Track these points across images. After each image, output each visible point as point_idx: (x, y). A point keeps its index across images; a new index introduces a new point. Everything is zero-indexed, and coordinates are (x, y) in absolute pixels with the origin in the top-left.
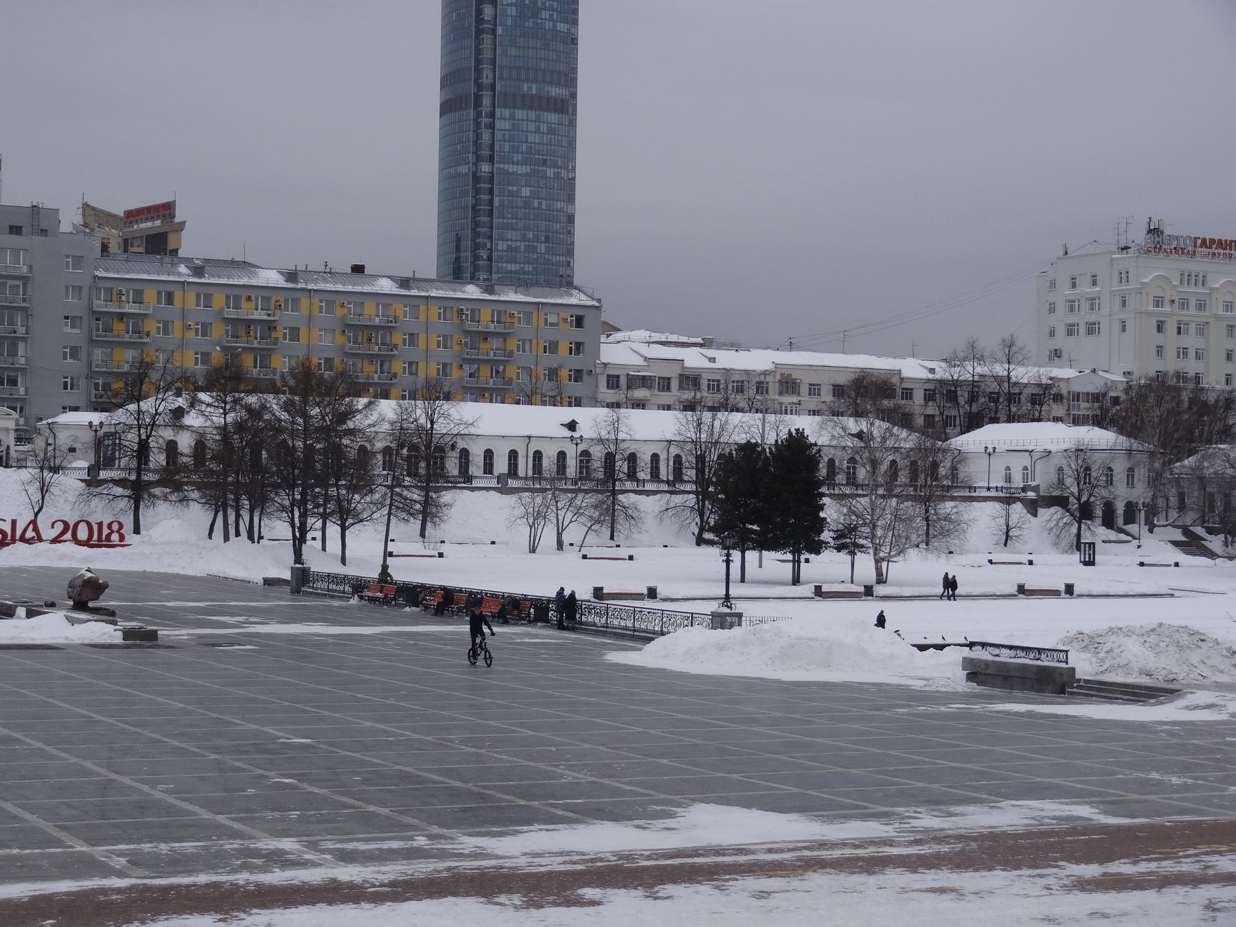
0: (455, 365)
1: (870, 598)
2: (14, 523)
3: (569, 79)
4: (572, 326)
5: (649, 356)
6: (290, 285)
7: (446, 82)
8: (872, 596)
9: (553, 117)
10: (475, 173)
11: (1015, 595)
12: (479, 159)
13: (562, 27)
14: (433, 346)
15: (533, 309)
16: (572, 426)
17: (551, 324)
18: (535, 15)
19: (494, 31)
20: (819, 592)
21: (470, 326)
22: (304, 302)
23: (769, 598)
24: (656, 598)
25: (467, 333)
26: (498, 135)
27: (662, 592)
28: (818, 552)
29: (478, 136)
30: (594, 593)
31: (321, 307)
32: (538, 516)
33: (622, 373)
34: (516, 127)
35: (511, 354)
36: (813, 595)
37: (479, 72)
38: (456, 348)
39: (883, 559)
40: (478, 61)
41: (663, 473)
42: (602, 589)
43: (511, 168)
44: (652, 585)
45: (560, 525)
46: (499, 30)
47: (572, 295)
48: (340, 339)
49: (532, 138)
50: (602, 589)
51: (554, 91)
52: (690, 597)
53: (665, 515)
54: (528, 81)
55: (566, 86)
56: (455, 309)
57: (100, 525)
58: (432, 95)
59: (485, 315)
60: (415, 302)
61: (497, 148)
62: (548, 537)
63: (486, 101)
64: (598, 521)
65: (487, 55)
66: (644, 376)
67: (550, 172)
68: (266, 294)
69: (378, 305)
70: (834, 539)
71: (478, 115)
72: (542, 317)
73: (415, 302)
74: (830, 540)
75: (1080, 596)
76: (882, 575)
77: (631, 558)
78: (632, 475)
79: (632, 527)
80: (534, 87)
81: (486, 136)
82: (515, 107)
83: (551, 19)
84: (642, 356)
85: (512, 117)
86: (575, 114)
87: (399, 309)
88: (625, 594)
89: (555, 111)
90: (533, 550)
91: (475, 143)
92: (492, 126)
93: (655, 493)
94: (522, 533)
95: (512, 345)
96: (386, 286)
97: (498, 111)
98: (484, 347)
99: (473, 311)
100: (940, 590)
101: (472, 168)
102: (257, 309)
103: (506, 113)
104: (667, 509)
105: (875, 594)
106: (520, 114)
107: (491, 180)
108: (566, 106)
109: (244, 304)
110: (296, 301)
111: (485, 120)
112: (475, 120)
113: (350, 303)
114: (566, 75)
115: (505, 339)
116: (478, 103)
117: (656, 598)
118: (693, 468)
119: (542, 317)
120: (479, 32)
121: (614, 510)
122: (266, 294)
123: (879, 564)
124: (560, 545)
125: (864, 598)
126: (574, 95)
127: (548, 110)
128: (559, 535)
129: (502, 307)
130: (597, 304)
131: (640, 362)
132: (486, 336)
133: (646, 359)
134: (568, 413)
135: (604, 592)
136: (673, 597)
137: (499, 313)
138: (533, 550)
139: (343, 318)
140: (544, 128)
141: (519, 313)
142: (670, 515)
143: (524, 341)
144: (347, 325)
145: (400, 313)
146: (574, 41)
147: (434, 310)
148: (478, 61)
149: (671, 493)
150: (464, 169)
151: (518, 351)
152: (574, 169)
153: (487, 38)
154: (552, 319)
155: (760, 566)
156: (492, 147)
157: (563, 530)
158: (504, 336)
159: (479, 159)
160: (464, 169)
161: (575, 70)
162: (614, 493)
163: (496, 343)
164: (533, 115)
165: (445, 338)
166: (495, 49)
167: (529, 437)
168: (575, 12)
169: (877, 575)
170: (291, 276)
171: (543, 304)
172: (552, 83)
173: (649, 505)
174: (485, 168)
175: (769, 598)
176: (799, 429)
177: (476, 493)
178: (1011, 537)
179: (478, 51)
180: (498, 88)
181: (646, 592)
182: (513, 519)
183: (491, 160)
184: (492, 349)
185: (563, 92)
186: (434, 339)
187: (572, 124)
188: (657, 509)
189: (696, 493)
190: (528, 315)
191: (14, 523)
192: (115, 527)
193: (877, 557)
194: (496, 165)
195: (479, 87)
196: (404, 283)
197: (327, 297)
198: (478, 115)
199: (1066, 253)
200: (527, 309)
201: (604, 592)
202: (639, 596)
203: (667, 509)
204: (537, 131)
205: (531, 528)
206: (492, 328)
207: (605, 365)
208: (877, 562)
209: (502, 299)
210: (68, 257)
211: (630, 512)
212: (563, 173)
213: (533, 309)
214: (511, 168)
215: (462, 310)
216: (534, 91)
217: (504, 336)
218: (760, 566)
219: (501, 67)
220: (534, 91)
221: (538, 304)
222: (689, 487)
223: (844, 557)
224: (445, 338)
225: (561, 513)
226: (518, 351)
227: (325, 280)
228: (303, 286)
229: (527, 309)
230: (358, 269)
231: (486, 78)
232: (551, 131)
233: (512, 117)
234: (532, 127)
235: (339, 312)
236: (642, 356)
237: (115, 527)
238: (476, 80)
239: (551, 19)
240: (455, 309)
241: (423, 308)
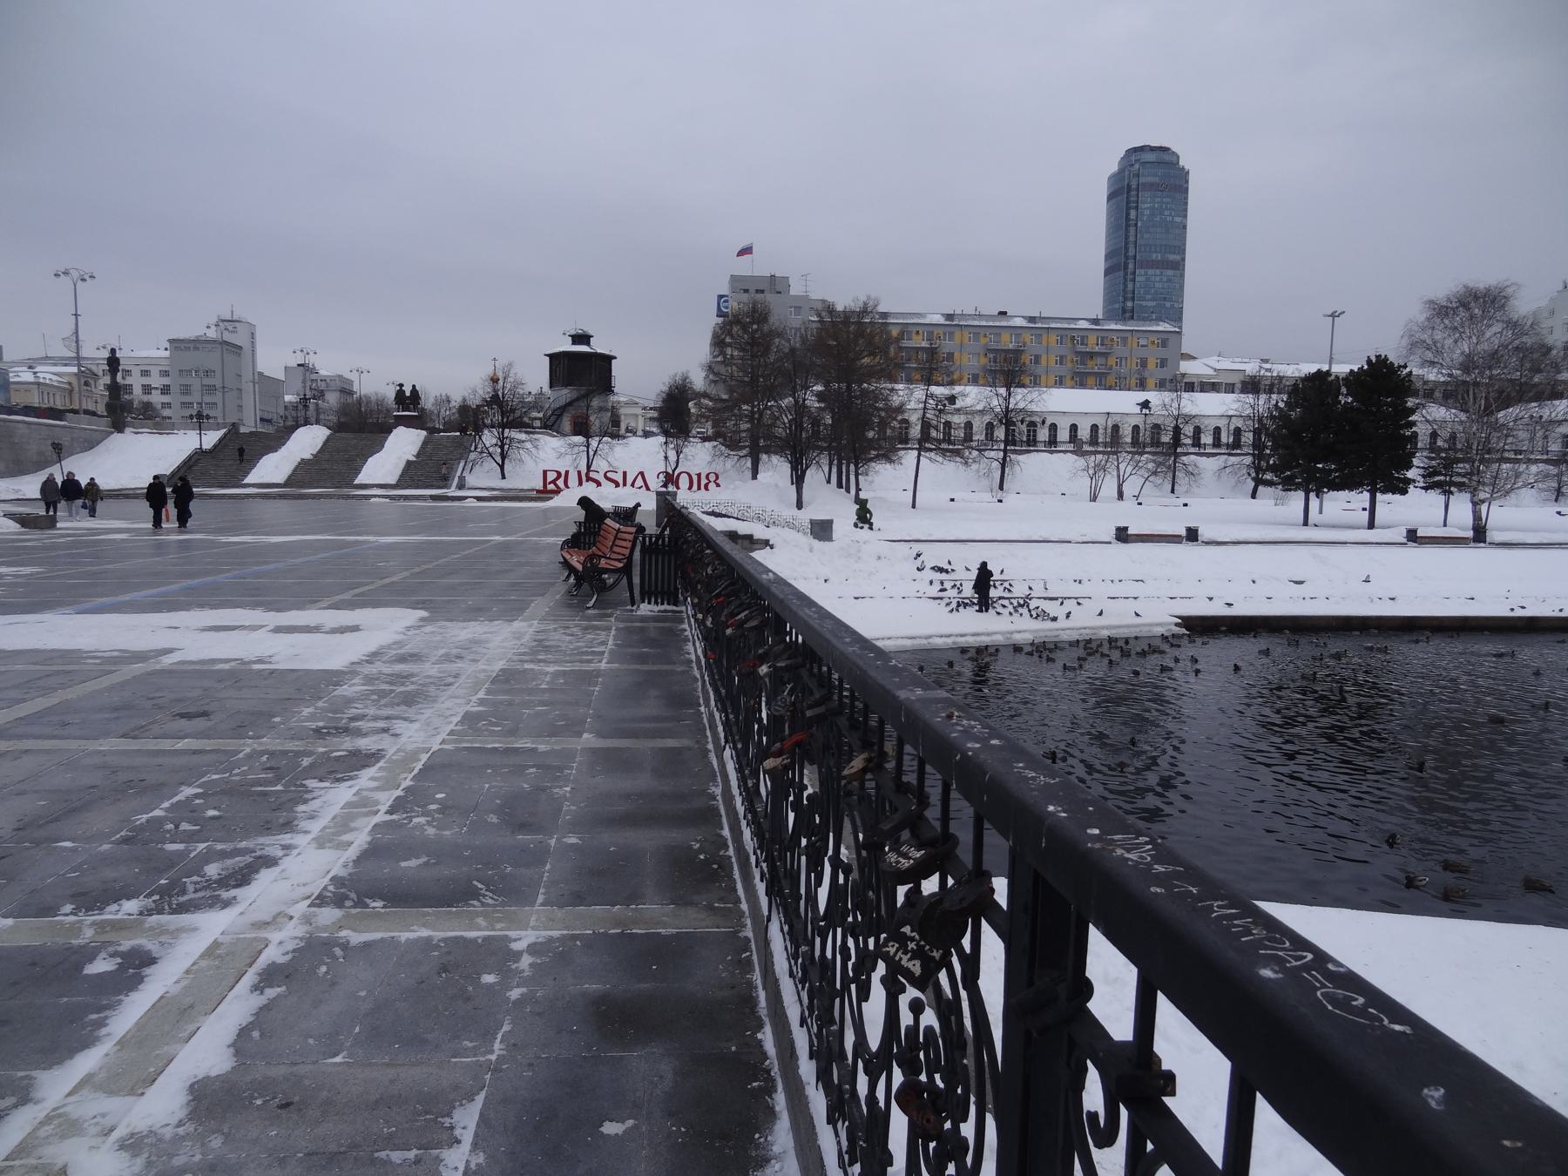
0: (1068, 377)
1: (1482, 545)
2: (625, 474)
3: (1181, 250)
4: (1158, 347)
5: (1218, 368)
6: (948, 323)
7: (1108, 257)
8: (1485, 542)
9: (1170, 272)
10: (1123, 308)
11: (1406, 544)
12: (1125, 299)
13: (1178, 219)
14: (1052, 363)
15: (1128, 335)
16: (1145, 405)
17: (1142, 346)
18: (1161, 214)
19: (1136, 225)
20: (1412, 536)
21: (1080, 348)
22: (957, 335)
23: (1346, 543)
24: (1197, 541)
25: (1077, 353)
26: (1137, 285)
27: (1205, 533)
28: (1404, 492)
29: (1125, 286)
30: (1116, 535)
31: (970, 337)
32: (1100, 468)
33: (1195, 380)
34: (1148, 280)
35: (1111, 368)
36: (1405, 540)
37: (1126, 249)
38: (1069, 365)
39: (1483, 501)
40: (1126, 244)
41: (1224, 439)
42: (1126, 529)
43: (1144, 303)
44: (1191, 525)
45: (1121, 477)
46: (1139, 224)
47: (1159, 325)
48: (984, 361)
49: (1157, 285)
50: (1126, 529)
51: (1172, 257)
52: (1241, 540)
53: (1223, 473)
54: (1156, 252)
55: (1179, 253)
56: (1069, 336)
57: (699, 475)
58: (1099, 264)
59: (1092, 339)
60: (1039, 332)
61: (1136, 292)
62: (1109, 487)
63: (1131, 266)
64: (1155, 473)
65: (1132, 239)
66: (1214, 383)
67: (1168, 304)
68: (931, 329)
69: (1011, 336)
70: (1424, 476)
71: (1126, 274)
72: (1135, 340)
73: (1039, 332)
74: (1419, 478)
75: (1207, 543)
76: (1481, 520)
77: (1186, 505)
78: (1197, 442)
79: (1191, 483)
80: (1159, 255)
81: (1130, 286)
82: (1147, 268)
83: (1170, 215)
84: (1212, 368)
85: (1146, 274)
86: (1184, 270)
87: (1027, 337)
88: (1158, 535)
89: (1172, 269)
90: (1094, 498)
91: (1123, 291)
92: (1134, 280)
93: (1214, 455)
94: (1084, 483)
95: (1112, 361)
96: (1019, 322)
97: (1137, 271)
98: (1090, 363)
99: (1083, 337)
100: (1470, 534)
101: (1122, 305)
102: (923, 340)
103: (1143, 272)
104: (1225, 468)
105: (1488, 540)
106: (1151, 272)
107: (1132, 311)
108: (1179, 266)
109: (914, 336)
110: (952, 334)
111: (1130, 277)
112: (1124, 277)
113: (990, 334)
114: (1180, 247)
115: (1107, 358)
116: (1126, 267)
117: (1197, 541)
118: (1251, 431)
119: (1135, 340)
120: (1127, 226)
121: (1175, 468)
122: (931, 329)
123: (1478, 507)
124: (1121, 496)
125: (1472, 544)
126: (1183, 259)
127: (1167, 268)
128: (1120, 487)
129: (1103, 334)
130: (1177, 330)
131: (1211, 372)
132: (1092, 355)
133: (1215, 370)
134: (1142, 396)
135: (1130, 532)
136: (1220, 540)
137: (1103, 338)
138: (1094, 498)
139: (986, 344)
140: (1165, 279)
141: (1118, 338)
142: (1228, 472)
143: (1121, 359)
144: (988, 350)
145: (1028, 340)
146: (1185, 227)
147: (1053, 338)
148: (1126, 244)
149: (1229, 454)
150: (1117, 306)
151: (1117, 365)
152: (1182, 302)
153: (1132, 230)
154: (1143, 342)
155: (1321, 512)
156: (1134, 291)
157: (1123, 482)
158: (1105, 355)
159: (1125, 299)
160: (1117, 306)
161: (1185, 244)
162: (1177, 456)
163: (1100, 360)
164: (1158, 272)
165: (1061, 357)
166: (1136, 236)
167: (1108, 413)
168: (1186, 210)
169: (1474, 520)
170: (949, 317)
171: (1136, 331)
172: (1170, 253)
173: (1208, 465)
174: (1129, 304)
175: (1346, 543)
176: (1380, 356)
177: (1055, 454)
178: (1563, 494)
179: (1127, 237)
180: (1138, 257)
181: (1183, 533)
182: (1074, 471)
183: (1133, 299)
184: (1096, 365)
185: (1178, 257)
186: (1053, 359)
187: (1182, 276)
188: (1216, 468)
189: (1253, 455)
190: (1125, 340)
191: (625, 474)
192: (712, 477)
193: (1476, 499)
194: (1136, 302)
195: (1127, 257)
196: (1032, 319)
197: (974, 330)
198: (1126, 274)
199: (1566, 287)
200: (1125, 335)
201: (1130, 532)
202: (1175, 539)
203: (1225, 468)
204: (1161, 281)
205: (1092, 478)
206: (1097, 349)
207: (1183, 375)
208: (1475, 504)
209: (1104, 328)
210: (791, 307)
211: (1190, 469)
212: (1176, 305)
213: (1128, 335)
214: (1144, 303)
215: (1074, 337)
216: (1159, 258)
217: (1105, 355)
218: (1321, 512)
219: (1140, 245)
220: (1159, 258)
221: (1132, 331)
222: (1245, 450)
223: (1435, 498)
224: (1061, 357)
225: (1122, 467)
226: (1117, 365)
227: (974, 319)
228: (957, 323)
229: (1125, 335)
230: (1003, 313)
231: (1131, 252)
232: (1169, 281)
233: (1146, 274)
234: (1158, 279)
235: (983, 341)
236: (1212, 368)
237: (712, 477)
238: (1125, 254)
239: (1170, 215)
240: (1069, 336)
241: (1045, 337)
